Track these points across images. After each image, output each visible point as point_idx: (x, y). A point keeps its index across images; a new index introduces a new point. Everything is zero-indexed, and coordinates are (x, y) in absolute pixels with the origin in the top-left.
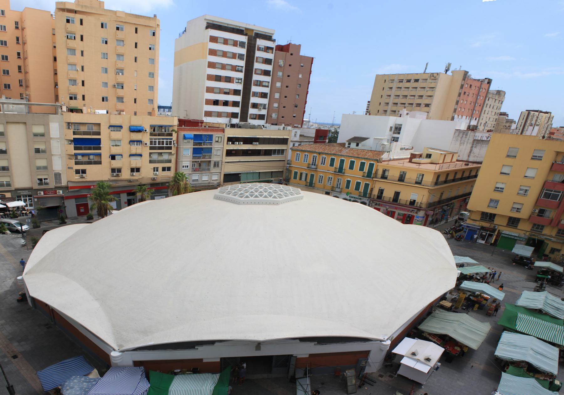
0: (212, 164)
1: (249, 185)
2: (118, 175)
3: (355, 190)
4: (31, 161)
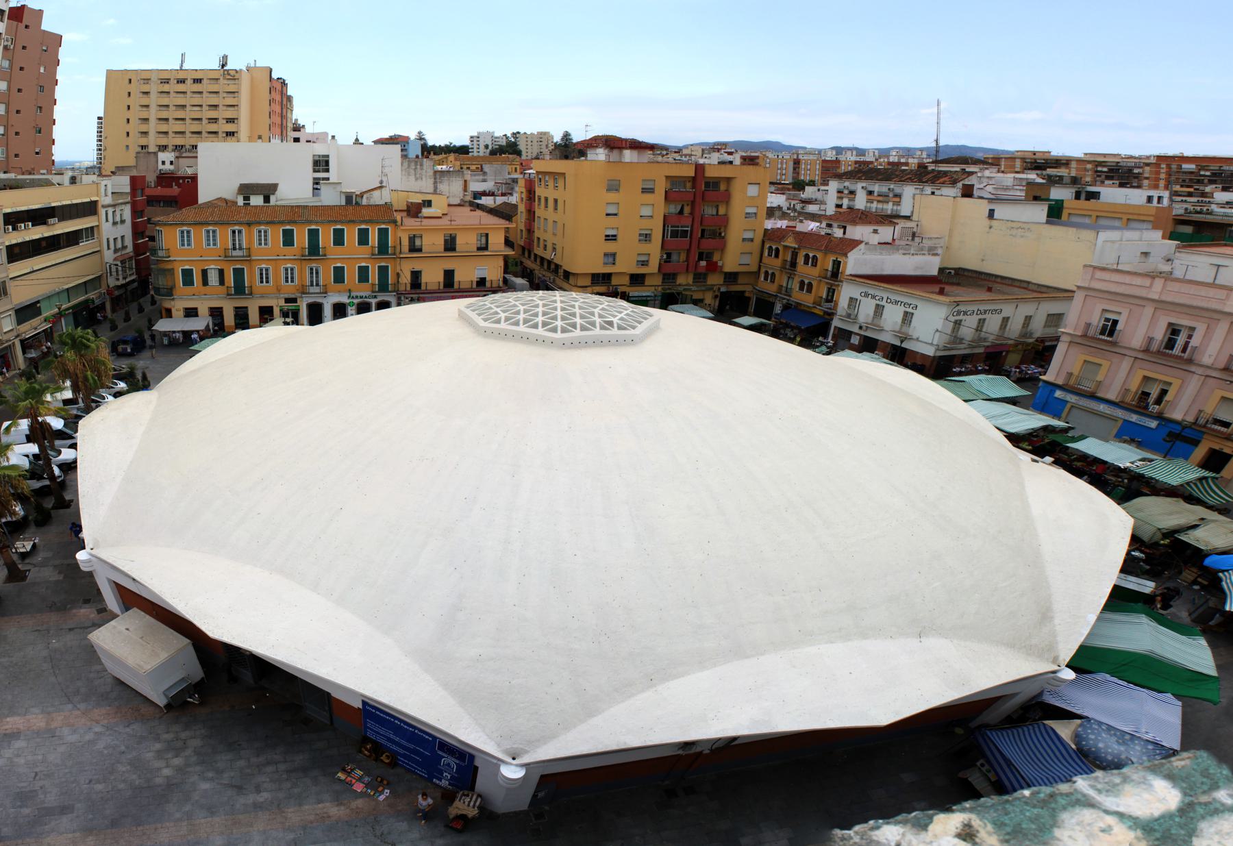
3: (359, 282)
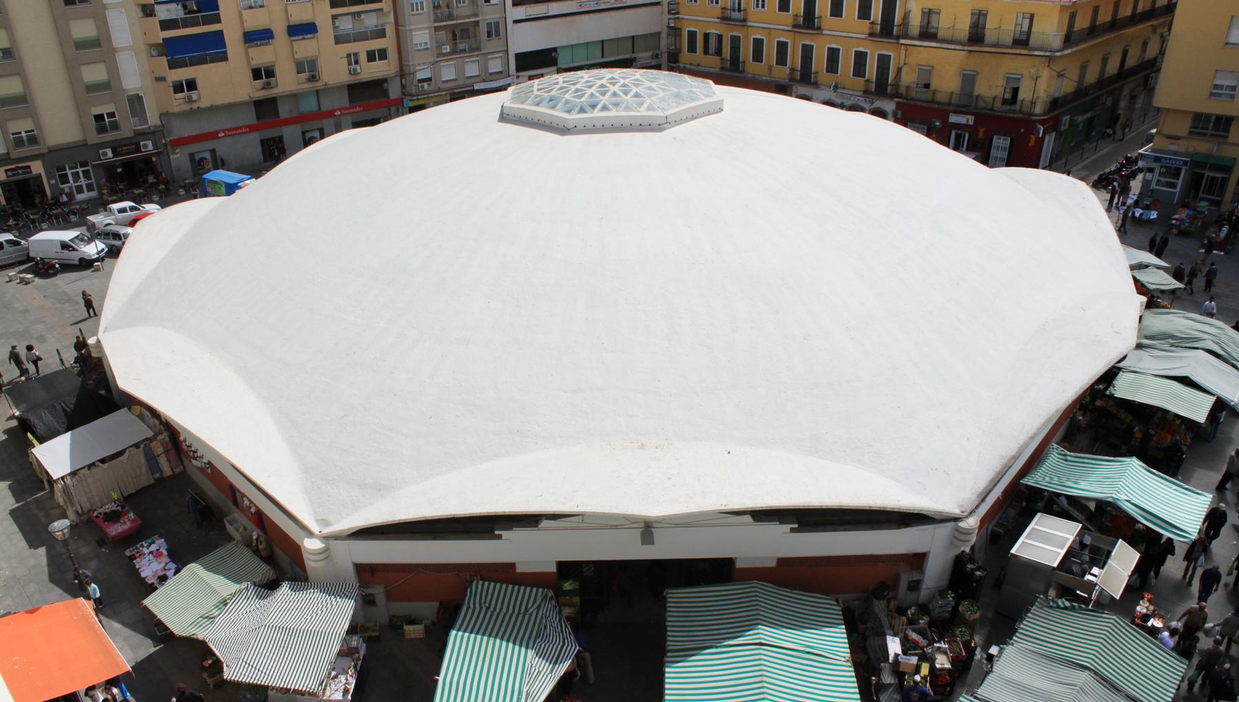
0: (483, 29)
1: (582, 78)
2: (268, 84)
4: (72, 70)
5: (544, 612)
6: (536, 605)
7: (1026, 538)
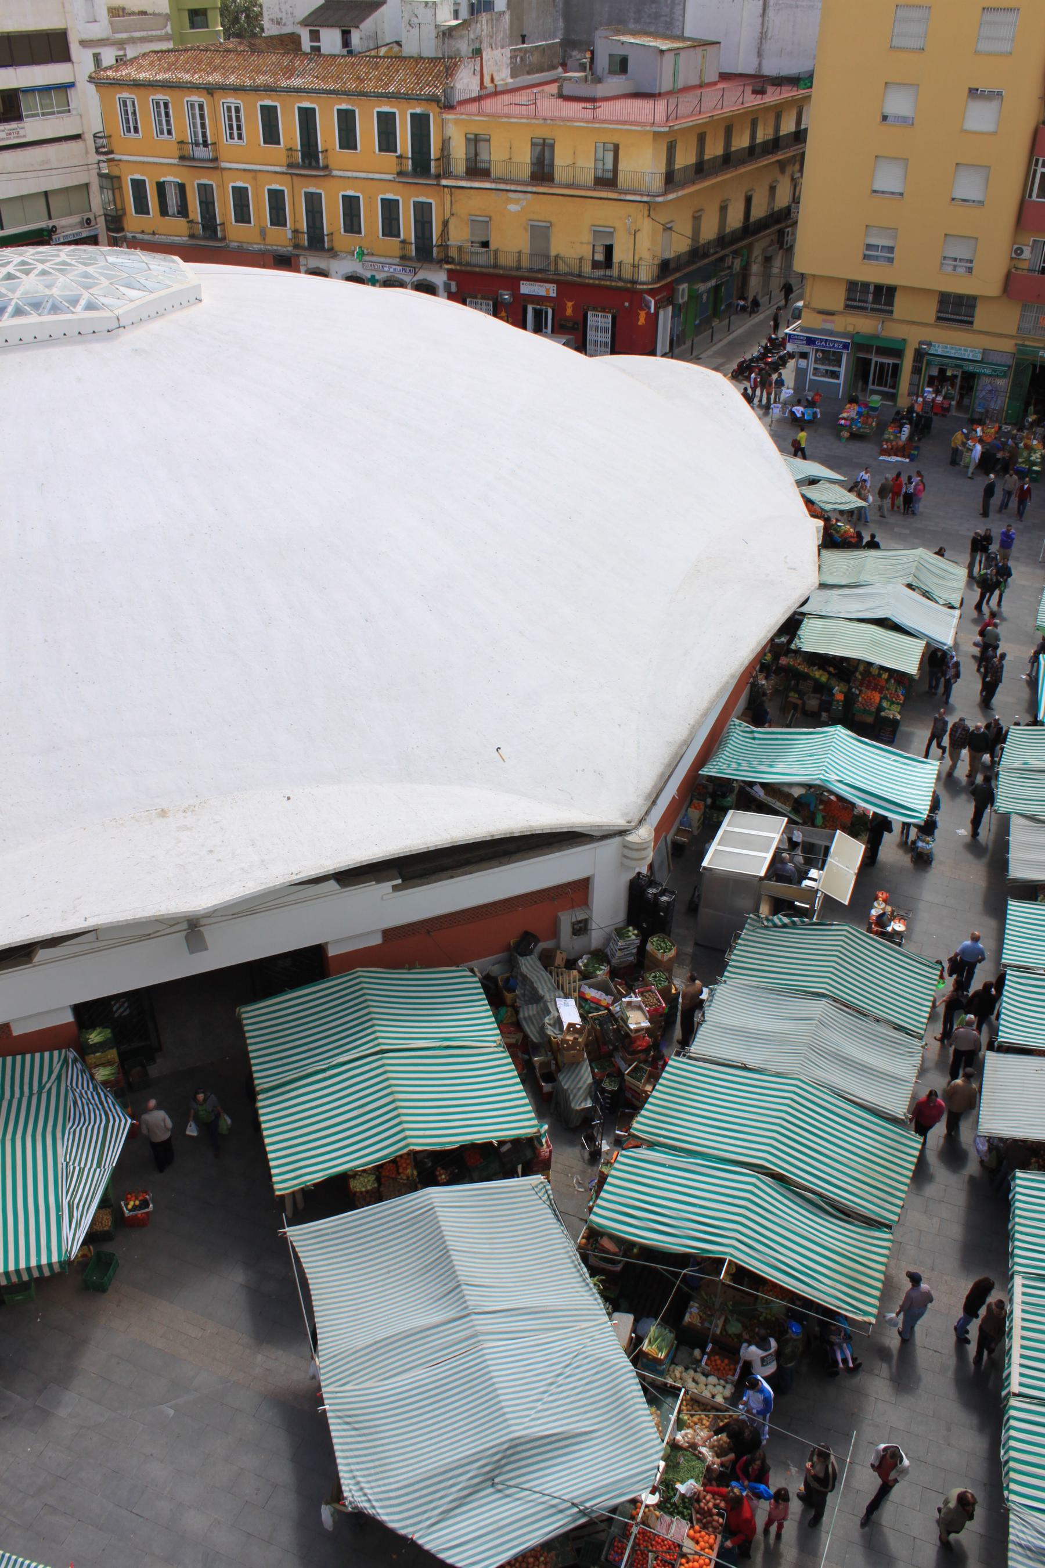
5: (69, 1084)
6: (54, 1076)
7: (719, 844)
